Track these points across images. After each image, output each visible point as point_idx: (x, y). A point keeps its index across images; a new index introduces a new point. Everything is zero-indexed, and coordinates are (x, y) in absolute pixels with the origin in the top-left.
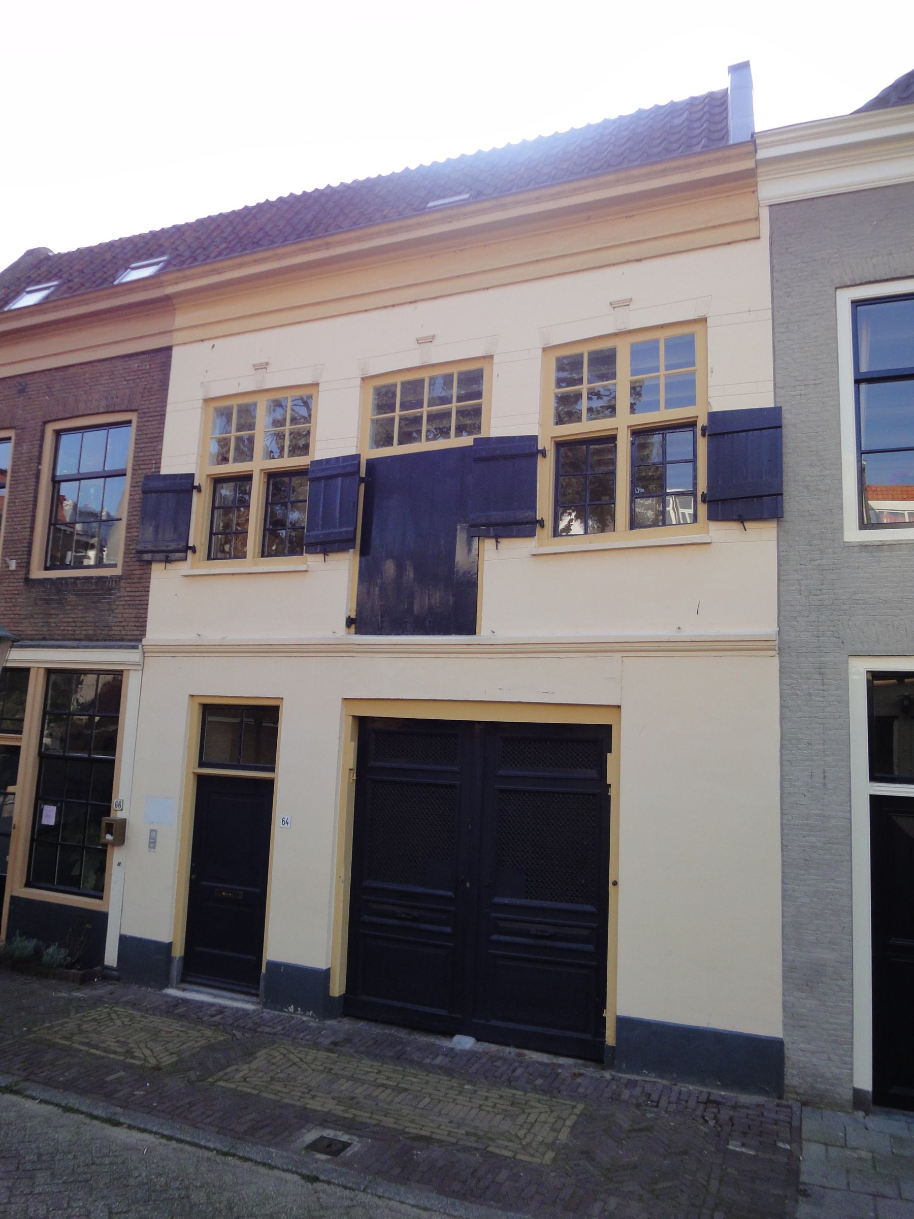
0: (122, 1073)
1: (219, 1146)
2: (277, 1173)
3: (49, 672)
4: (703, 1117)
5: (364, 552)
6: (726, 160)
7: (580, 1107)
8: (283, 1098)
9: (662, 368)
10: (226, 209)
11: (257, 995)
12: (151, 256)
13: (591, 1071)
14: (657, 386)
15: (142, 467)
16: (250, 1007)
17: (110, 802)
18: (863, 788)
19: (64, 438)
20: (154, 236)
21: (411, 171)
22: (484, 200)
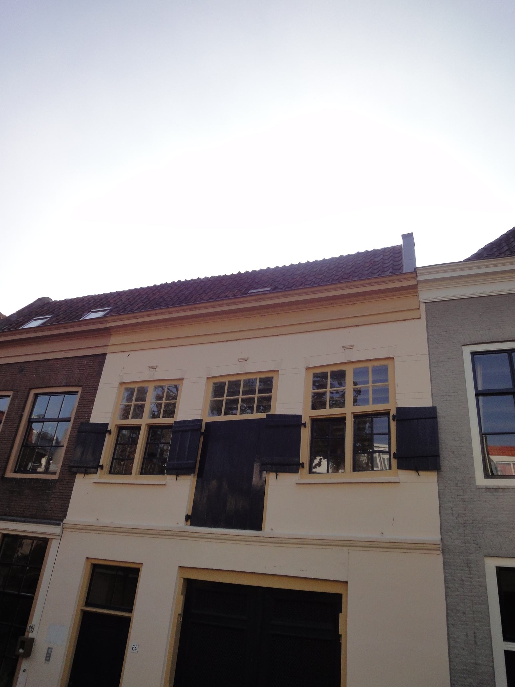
5: (199, 476)
6: (403, 280)
9: (370, 382)
10: (145, 285)
12: (102, 306)
14: (368, 391)
15: (80, 417)
19: (40, 398)
20: (106, 296)
21: (242, 274)
22: (278, 292)
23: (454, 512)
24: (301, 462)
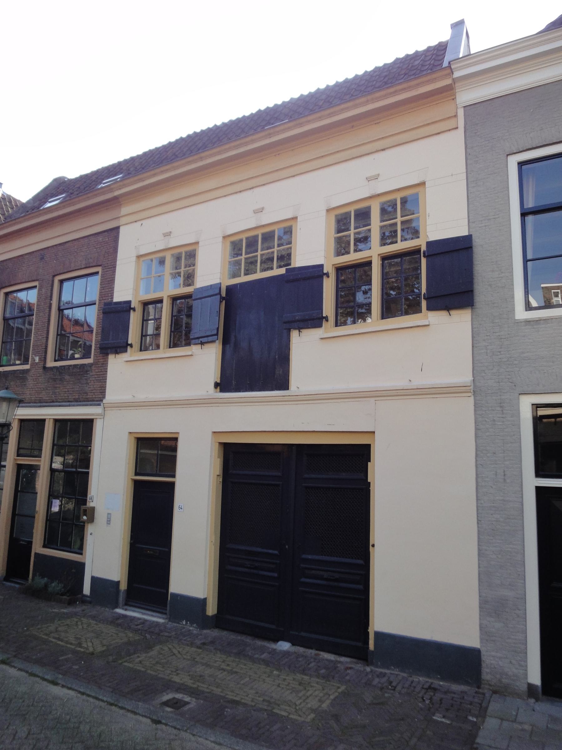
0: (70, 656)
1: (109, 700)
2: (138, 717)
3: (56, 421)
4: (423, 698)
5: (225, 342)
7: (343, 688)
8: (159, 674)
11: (165, 614)
13: (359, 666)
15: (104, 298)
16: (161, 621)
17: (87, 497)
18: (531, 482)
19: (65, 284)
23: (488, 351)
24: (324, 315)
